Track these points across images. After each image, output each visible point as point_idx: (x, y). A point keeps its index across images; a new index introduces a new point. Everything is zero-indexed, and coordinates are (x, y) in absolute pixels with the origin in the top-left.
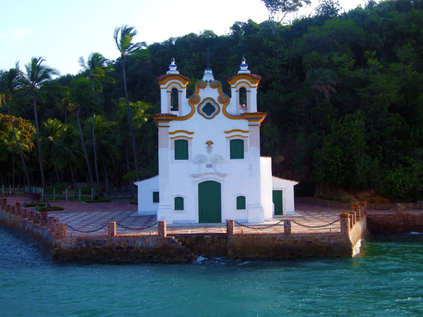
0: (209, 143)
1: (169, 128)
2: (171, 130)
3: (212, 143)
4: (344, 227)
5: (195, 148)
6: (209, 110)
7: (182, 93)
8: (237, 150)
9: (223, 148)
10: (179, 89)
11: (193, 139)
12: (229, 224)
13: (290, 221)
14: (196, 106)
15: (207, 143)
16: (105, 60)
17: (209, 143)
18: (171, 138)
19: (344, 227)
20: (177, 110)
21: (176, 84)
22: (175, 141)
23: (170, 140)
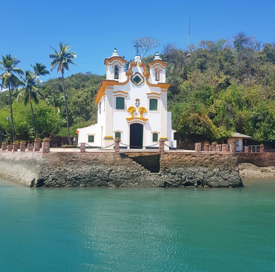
0: (138, 100)
1: (113, 89)
2: (114, 90)
3: (139, 100)
4: (79, 148)
5: (129, 103)
6: (137, 80)
7: (122, 68)
8: (153, 104)
9: (145, 104)
10: (120, 66)
11: (127, 97)
12: (83, 147)
13: (179, 147)
14: (130, 77)
15: (136, 100)
16: (6, 88)
17: (138, 100)
18: (114, 96)
19: (79, 148)
20: (118, 78)
21: (115, 63)
22: (117, 98)
23: (113, 96)
